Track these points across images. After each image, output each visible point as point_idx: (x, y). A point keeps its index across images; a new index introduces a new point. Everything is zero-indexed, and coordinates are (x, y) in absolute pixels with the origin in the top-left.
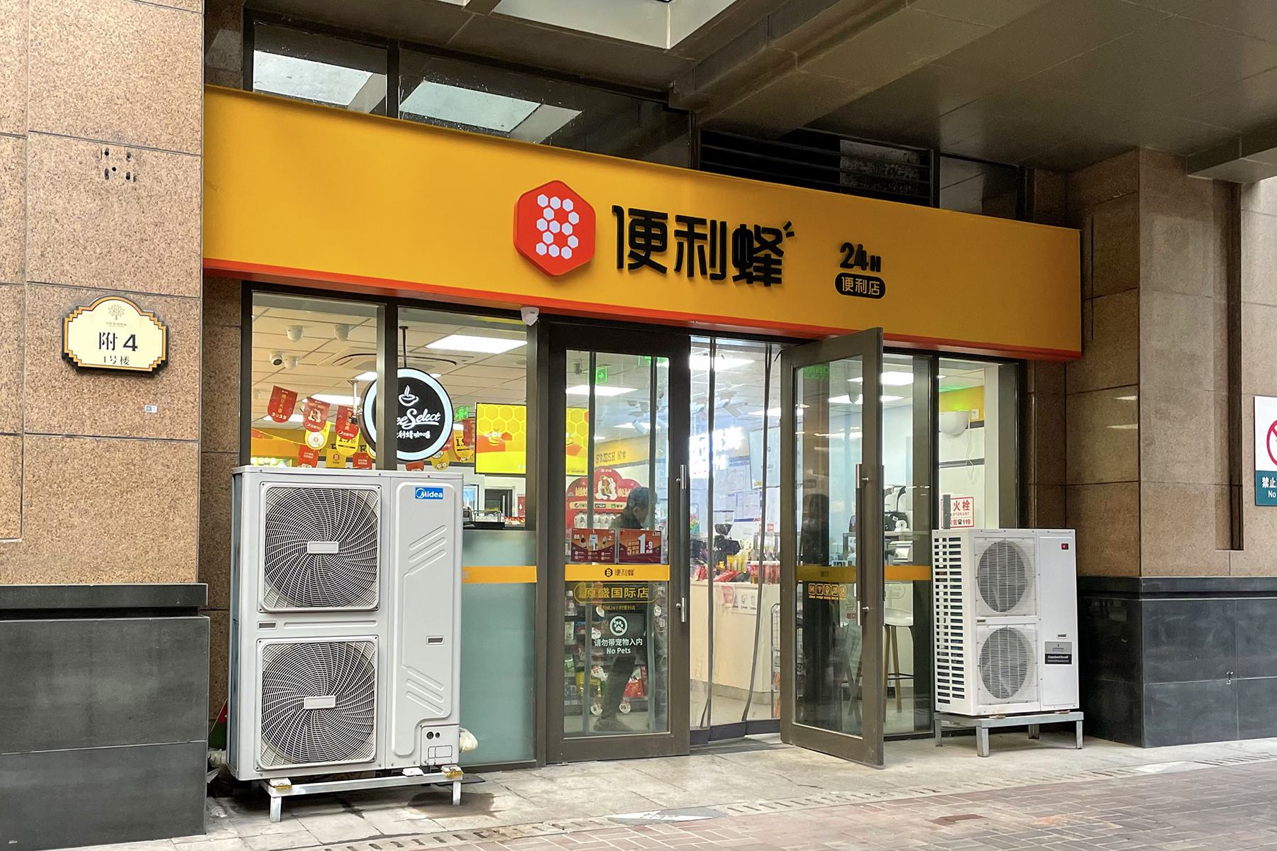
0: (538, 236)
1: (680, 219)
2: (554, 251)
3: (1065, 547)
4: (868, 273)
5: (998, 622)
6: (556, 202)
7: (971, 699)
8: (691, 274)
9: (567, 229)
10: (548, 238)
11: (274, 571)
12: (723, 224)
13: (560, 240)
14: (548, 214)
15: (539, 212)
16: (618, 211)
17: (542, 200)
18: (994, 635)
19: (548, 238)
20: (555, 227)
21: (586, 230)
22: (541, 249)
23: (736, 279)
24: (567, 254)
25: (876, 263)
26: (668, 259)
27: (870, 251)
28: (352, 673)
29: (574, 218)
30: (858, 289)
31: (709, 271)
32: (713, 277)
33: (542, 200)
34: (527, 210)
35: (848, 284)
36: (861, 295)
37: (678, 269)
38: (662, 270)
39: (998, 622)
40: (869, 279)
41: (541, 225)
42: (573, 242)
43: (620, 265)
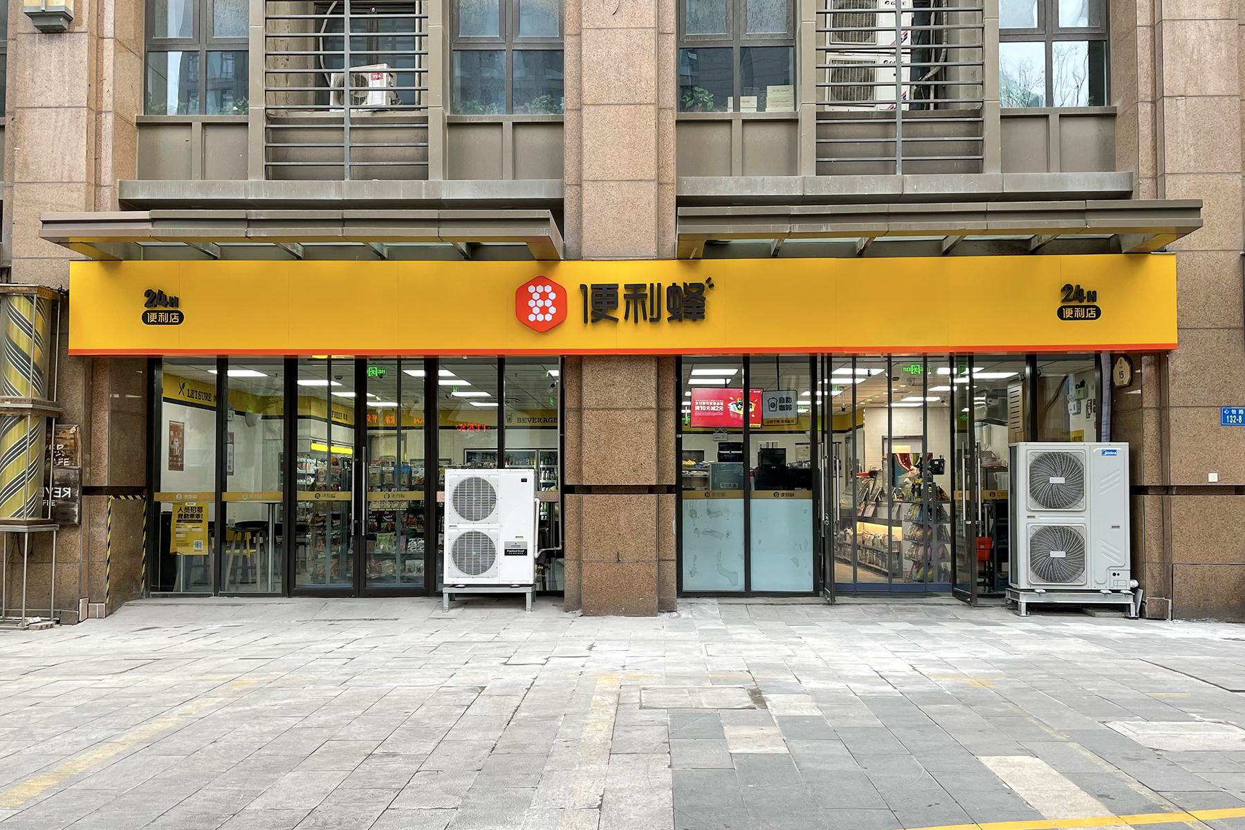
0: (530, 310)
1: (626, 286)
2: (540, 318)
3: (524, 480)
4: (1085, 303)
5: (467, 526)
6: (540, 289)
7: (452, 575)
8: (636, 321)
9: (548, 303)
10: (536, 310)
11: (1034, 493)
12: (659, 285)
13: (544, 310)
14: (536, 296)
15: (530, 296)
16: (583, 287)
17: (531, 289)
18: (462, 537)
19: (536, 310)
20: (540, 303)
21: (561, 303)
22: (532, 318)
23: (669, 319)
24: (549, 318)
25: (175, 302)
26: (620, 313)
27: (169, 293)
28: (1072, 540)
29: (553, 296)
30: (1088, 315)
31: (649, 316)
32: (651, 320)
33: (531, 289)
34: (522, 295)
35: (153, 317)
36: (1080, 319)
37: (626, 317)
38: (617, 320)
39: (467, 526)
40: (169, 312)
41: (532, 303)
42: (553, 310)
43: (586, 321)
